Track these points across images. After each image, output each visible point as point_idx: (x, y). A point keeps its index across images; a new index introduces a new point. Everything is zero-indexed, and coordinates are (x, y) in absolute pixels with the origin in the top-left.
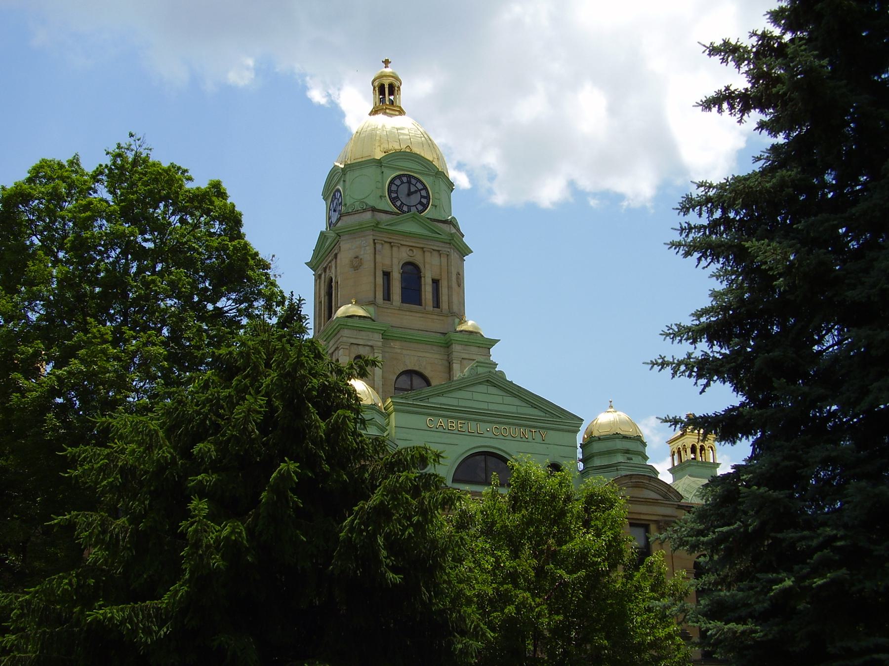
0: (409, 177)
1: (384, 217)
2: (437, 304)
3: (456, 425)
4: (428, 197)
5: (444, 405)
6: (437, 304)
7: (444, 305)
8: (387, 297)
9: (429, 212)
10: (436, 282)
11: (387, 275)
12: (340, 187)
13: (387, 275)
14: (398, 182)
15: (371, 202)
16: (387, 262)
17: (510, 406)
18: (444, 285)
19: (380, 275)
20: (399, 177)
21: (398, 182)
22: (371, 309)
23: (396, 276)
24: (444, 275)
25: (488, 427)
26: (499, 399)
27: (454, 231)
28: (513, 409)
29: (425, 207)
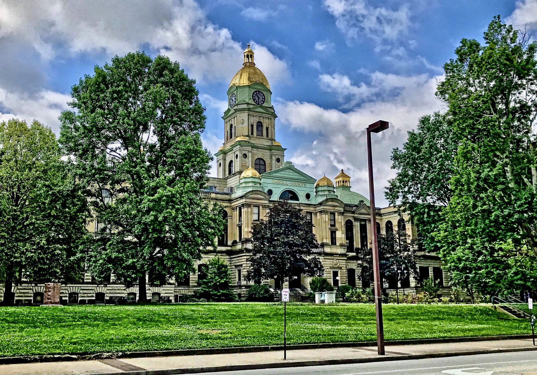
0: (259, 91)
1: (252, 106)
2: (267, 136)
3: (281, 182)
4: (264, 99)
5: (193, 305)
6: (267, 136)
7: (270, 136)
8: (252, 134)
9: (265, 105)
10: (267, 128)
11: (252, 126)
12: (235, 92)
13: (252, 126)
14: (255, 93)
15: (247, 100)
16: (252, 121)
17: (296, 176)
18: (270, 129)
19: (250, 126)
20: (256, 92)
21: (255, 93)
22: (248, 138)
23: (255, 127)
24: (270, 127)
25: (290, 182)
26: (292, 174)
27: (273, 111)
28: (296, 177)
29: (264, 102)
